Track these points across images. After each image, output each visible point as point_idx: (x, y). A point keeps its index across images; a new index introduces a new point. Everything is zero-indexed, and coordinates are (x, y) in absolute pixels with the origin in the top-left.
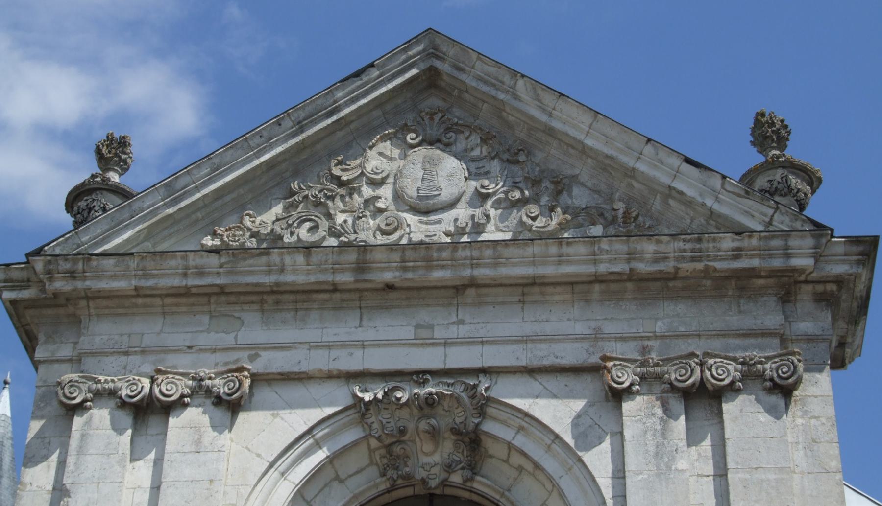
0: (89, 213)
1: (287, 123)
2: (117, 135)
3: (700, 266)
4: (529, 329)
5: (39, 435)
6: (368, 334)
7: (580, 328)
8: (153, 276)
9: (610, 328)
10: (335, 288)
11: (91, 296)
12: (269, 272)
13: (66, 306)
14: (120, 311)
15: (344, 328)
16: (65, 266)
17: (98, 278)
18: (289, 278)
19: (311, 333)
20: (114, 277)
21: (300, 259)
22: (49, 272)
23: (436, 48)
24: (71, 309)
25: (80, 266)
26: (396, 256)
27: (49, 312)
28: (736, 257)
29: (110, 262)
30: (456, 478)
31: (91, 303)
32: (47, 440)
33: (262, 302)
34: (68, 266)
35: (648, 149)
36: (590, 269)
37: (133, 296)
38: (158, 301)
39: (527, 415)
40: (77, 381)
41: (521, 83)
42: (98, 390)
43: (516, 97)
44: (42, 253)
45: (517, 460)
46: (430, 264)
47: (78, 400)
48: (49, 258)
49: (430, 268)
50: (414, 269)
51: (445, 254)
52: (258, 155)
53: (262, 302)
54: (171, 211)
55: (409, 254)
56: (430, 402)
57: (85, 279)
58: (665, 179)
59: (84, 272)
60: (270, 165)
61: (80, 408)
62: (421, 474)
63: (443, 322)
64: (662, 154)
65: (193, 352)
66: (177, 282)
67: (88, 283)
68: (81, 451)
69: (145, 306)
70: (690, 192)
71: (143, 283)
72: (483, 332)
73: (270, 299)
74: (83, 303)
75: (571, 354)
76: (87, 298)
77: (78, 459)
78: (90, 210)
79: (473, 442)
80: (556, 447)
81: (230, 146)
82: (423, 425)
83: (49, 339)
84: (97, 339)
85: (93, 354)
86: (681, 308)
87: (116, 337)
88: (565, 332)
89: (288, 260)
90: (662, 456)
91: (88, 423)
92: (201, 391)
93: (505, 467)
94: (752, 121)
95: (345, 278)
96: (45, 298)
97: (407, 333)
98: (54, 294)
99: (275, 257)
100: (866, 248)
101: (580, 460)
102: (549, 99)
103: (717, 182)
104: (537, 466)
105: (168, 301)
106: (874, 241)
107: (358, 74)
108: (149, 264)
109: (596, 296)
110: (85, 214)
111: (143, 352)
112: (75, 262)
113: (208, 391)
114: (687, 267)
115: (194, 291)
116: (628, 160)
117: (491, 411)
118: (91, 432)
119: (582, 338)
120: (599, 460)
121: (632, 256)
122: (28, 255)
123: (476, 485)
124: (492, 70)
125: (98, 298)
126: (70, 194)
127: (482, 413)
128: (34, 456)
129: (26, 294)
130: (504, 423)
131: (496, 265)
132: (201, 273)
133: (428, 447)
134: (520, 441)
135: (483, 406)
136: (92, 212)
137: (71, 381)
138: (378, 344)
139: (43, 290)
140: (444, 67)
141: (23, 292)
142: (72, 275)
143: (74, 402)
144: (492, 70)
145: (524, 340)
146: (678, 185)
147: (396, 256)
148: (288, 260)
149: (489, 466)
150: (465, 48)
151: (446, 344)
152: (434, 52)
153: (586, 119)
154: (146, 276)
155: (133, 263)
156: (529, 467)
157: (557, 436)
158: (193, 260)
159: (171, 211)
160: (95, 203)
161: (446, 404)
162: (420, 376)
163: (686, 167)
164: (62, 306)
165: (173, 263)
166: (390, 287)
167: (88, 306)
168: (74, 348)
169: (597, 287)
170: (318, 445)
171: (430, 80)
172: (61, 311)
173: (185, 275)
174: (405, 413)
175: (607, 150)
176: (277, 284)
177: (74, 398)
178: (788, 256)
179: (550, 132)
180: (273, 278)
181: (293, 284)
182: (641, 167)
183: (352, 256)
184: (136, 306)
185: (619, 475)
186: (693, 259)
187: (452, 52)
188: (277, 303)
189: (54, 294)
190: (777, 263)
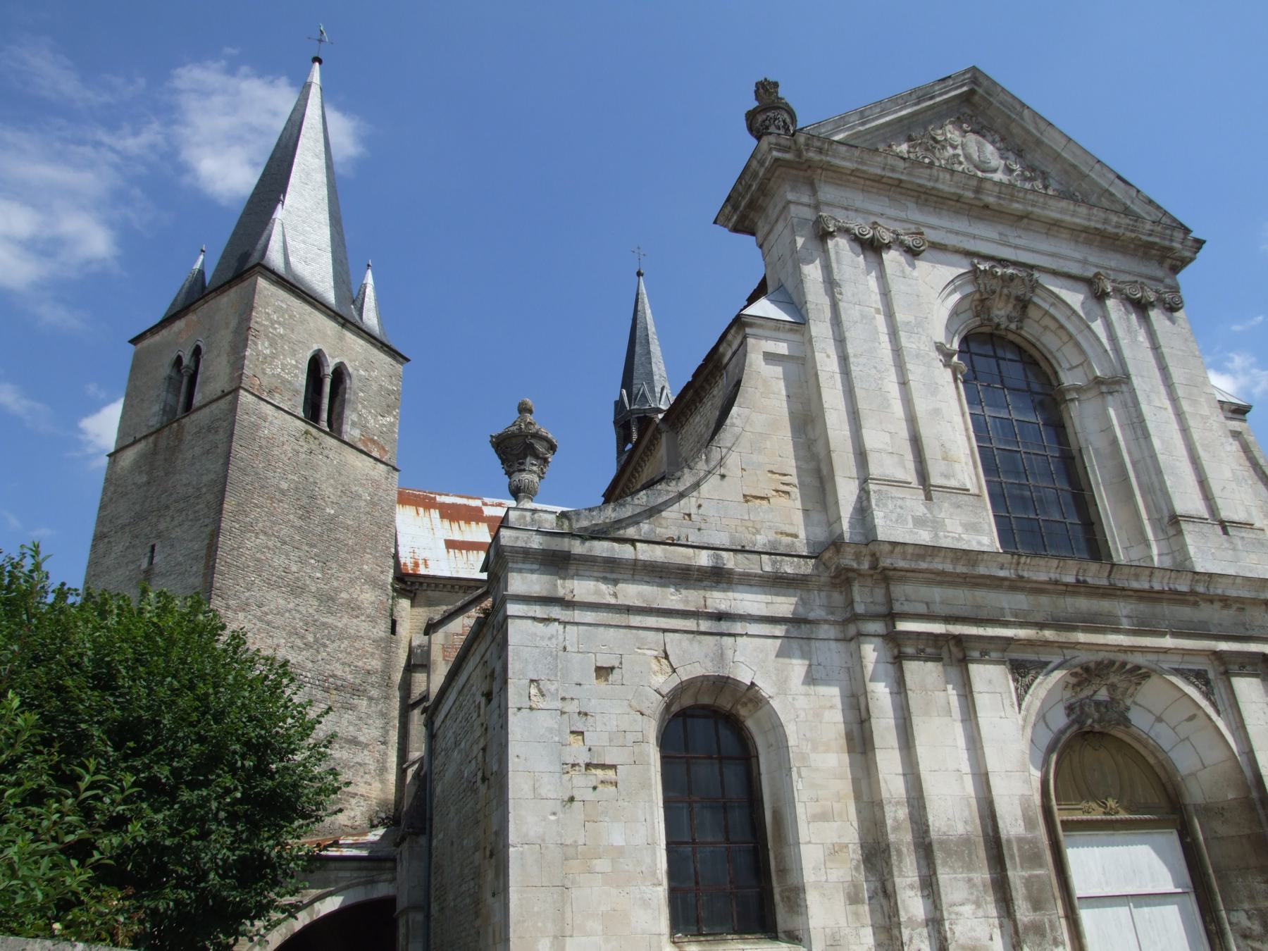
1: (914, 96)
3: (1133, 235)
4: (1053, 249)
5: (804, 246)
6: (972, 230)
7: (1078, 255)
8: (866, 164)
9: (1091, 259)
10: (959, 199)
11: (828, 168)
12: (929, 180)
15: (961, 225)
17: (834, 156)
18: (940, 186)
19: (945, 223)
20: (844, 159)
21: (948, 177)
22: (807, 145)
23: (976, 78)
24: (809, 173)
25: (826, 146)
26: (997, 189)
27: (794, 172)
28: (1150, 235)
30: (1013, 326)
33: (919, 197)
34: (819, 144)
35: (1097, 166)
36: (1085, 223)
38: (862, 181)
39: (1057, 297)
41: (1026, 111)
43: (1022, 119)
45: (1047, 321)
46: (1013, 198)
49: (1012, 201)
50: (1004, 199)
51: (1021, 195)
52: (901, 110)
53: (919, 197)
54: (861, 128)
55: (1003, 189)
56: (1012, 278)
57: (827, 155)
58: (1106, 185)
60: (901, 119)
61: (831, 235)
62: (996, 320)
63: (1014, 236)
64: (1105, 171)
65: (889, 219)
66: (879, 172)
67: (829, 159)
68: (838, 262)
69: (854, 182)
70: (1119, 195)
71: (860, 167)
72: (1033, 245)
73: (923, 196)
74: (819, 171)
75: (1075, 269)
79: (1023, 305)
80: (1073, 318)
81: (891, 100)
82: (1005, 291)
83: (793, 189)
85: (828, 204)
86: (1119, 256)
88: (1073, 256)
89: (941, 175)
90: (1129, 330)
92: (898, 243)
93: (1036, 325)
95: (970, 194)
97: (995, 236)
99: (935, 172)
100: (1199, 243)
101: (1089, 327)
102: (1042, 126)
103: (1134, 194)
104: (1062, 327)
105: (868, 183)
106: (1204, 242)
107: (943, 80)
108: (866, 156)
109: (1081, 239)
111: (856, 211)
112: (824, 143)
113: (902, 244)
114: (1128, 234)
115: (884, 180)
116: (1085, 170)
117: (1038, 291)
119: (1078, 261)
120: (1098, 326)
121: (1106, 221)
123: (1023, 333)
124: (1009, 100)
127: (1033, 290)
129: (788, 156)
130: (1043, 299)
131: (1043, 208)
132: (893, 170)
133: (1001, 305)
134: (1052, 311)
135: (1035, 286)
138: (982, 239)
140: (980, 91)
142: (820, 151)
144: (1009, 100)
145: (1053, 255)
146: (1112, 190)
147: (997, 189)
148: (941, 175)
149: (1027, 322)
150: (995, 83)
151: (1016, 247)
152: (974, 81)
153: (1064, 142)
154: (862, 163)
155: (857, 153)
156: (1053, 325)
157: (1074, 312)
158: (890, 161)
159: (861, 128)
161: (1016, 282)
162: (1003, 262)
163: (1117, 181)
165: (879, 159)
166: (986, 207)
169: (1084, 235)
170: (954, 291)
171: (967, 98)
172: (801, 173)
173: (884, 169)
174: (994, 282)
175: (1073, 161)
176: (933, 188)
178: (1171, 240)
179: (1039, 143)
180: (930, 184)
181: (942, 191)
182: (1093, 175)
183: (974, 183)
184: (848, 181)
185: (1113, 338)
186: (1132, 231)
187: (985, 83)
188: (926, 200)
190: (1167, 243)
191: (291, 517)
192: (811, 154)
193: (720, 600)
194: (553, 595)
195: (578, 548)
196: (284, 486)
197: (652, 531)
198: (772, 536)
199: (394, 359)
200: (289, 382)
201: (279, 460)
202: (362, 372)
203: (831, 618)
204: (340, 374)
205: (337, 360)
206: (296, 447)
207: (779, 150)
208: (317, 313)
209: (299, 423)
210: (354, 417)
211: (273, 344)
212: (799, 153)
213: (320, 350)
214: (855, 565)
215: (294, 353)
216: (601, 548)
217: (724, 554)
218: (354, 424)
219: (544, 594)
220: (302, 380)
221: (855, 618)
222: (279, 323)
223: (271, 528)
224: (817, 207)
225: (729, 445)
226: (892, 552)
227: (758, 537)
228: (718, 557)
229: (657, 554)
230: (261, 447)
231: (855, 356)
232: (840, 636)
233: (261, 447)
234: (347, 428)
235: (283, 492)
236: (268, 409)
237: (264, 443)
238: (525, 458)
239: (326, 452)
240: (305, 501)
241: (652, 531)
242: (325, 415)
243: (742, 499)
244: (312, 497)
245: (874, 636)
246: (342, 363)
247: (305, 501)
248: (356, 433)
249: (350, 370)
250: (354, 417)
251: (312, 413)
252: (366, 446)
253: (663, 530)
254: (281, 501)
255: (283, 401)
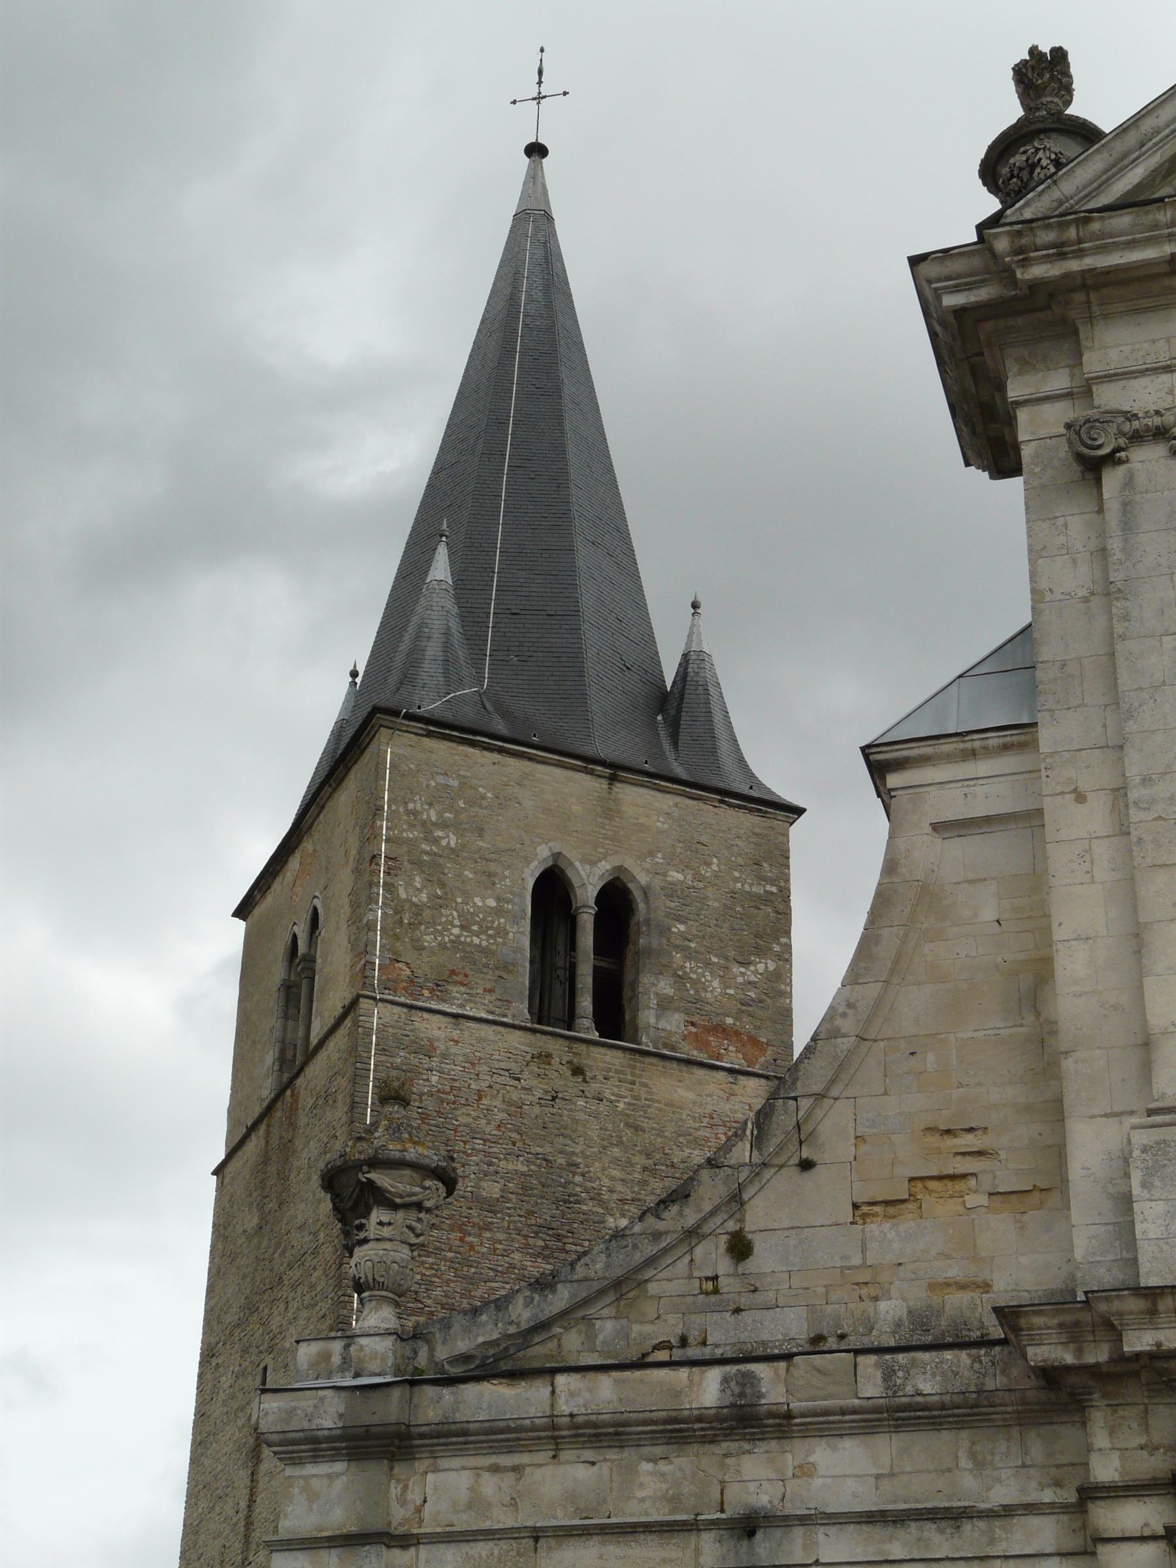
0: (1031, 173)
2: (1045, 48)
13: (1049, 307)
14: (1145, 303)
16: (1047, 237)
29: (1123, 221)
31: (1094, 296)
32: (1060, 521)
34: (1049, 237)
37: (1166, 275)
40: (1097, 420)
42: (1136, 431)
44: (1003, 221)
47: (1106, 450)
48: (1017, 227)
59: (1080, 241)
61: (1112, 459)
68: (1128, 526)
74: (1079, 297)
76: (1085, 287)
77: (1126, 541)
78: (1032, 167)
83: (1026, 365)
84: (1113, 354)
87: (1146, 346)
91: (1129, 483)
94: (1029, 596)
96: (1014, 299)
98: (1030, 287)
110: (1025, 175)
118: (1138, 498)
122: (980, 228)
125: (1106, 285)
126: (991, 148)
128: (1045, 548)
136: (1038, 170)
137: (1088, 421)
139: (1013, 282)
141: (975, 292)
143: (1101, 452)
160: (1040, 154)
164: (1041, 310)
167: (1089, 302)
168: (1072, 376)
177: (1099, 447)
189: (1030, 287)
191: (517, 1256)
192: (1038, 271)
193: (756, 1476)
194: (378, 1526)
195: (435, 1405)
196: (492, 1189)
197: (624, 1335)
198: (918, 1295)
199: (763, 814)
200: (485, 951)
201: (474, 1133)
202: (675, 876)
203: (1048, 1496)
204: (616, 900)
205: (605, 866)
206: (515, 1096)
207: (957, 289)
208: (542, 771)
209: (516, 1039)
210: (665, 986)
211: (433, 871)
212: (1006, 275)
213: (557, 856)
214: (1069, 1359)
215: (489, 879)
216: (484, 1400)
217: (761, 1370)
218: (665, 1005)
219: (354, 1529)
220: (519, 936)
221: (1090, 1494)
222: (444, 825)
223: (466, 1294)
224: (1084, 391)
225: (817, 1088)
226: (1153, 1312)
227: (883, 1306)
228: (749, 1380)
229: (603, 1395)
230: (424, 1117)
231: (1146, 781)
232: (1073, 1543)
233: (424, 1117)
234: (648, 1017)
235: (491, 1206)
236: (433, 1028)
237: (430, 1104)
238: (366, 1214)
239: (594, 1087)
240: (548, 1211)
241: (624, 1335)
242: (585, 1003)
243: (847, 1214)
244: (569, 1200)
245: (1142, 1539)
246: (620, 868)
247: (548, 1211)
248: (674, 1023)
249: (643, 878)
250: (665, 986)
251: (549, 1007)
252: (703, 1045)
253: (649, 1328)
254: (487, 1227)
255: (472, 998)
